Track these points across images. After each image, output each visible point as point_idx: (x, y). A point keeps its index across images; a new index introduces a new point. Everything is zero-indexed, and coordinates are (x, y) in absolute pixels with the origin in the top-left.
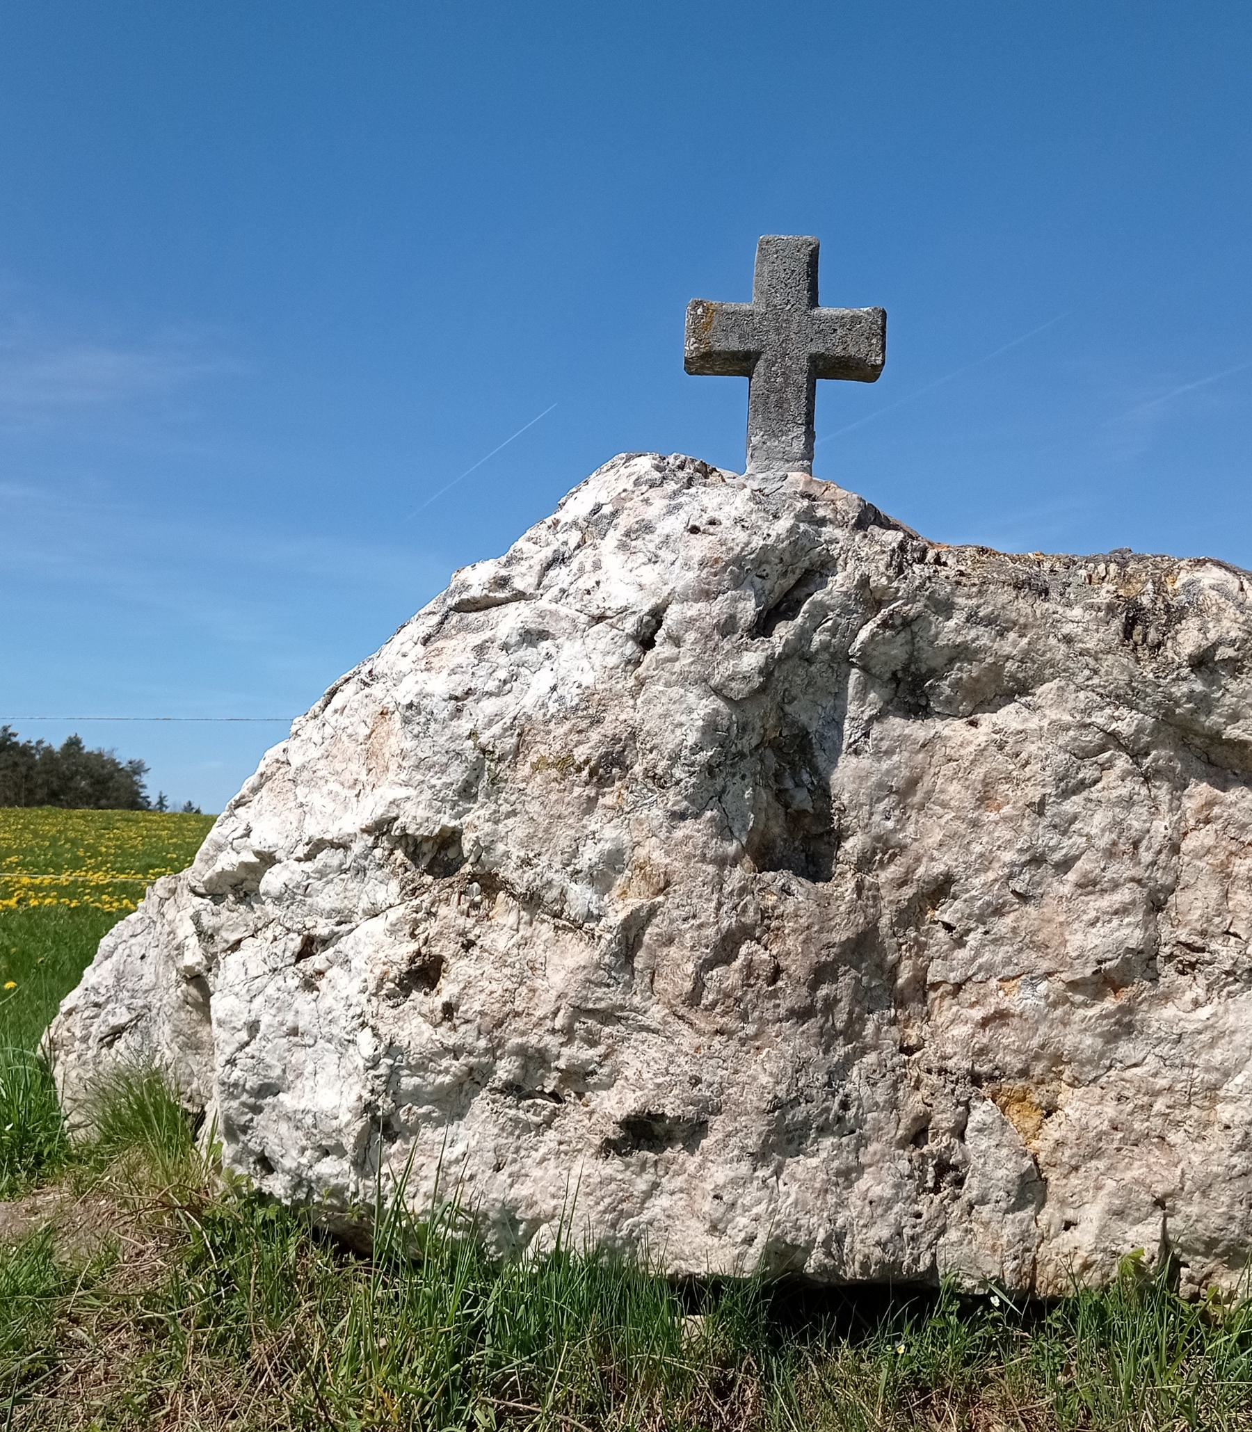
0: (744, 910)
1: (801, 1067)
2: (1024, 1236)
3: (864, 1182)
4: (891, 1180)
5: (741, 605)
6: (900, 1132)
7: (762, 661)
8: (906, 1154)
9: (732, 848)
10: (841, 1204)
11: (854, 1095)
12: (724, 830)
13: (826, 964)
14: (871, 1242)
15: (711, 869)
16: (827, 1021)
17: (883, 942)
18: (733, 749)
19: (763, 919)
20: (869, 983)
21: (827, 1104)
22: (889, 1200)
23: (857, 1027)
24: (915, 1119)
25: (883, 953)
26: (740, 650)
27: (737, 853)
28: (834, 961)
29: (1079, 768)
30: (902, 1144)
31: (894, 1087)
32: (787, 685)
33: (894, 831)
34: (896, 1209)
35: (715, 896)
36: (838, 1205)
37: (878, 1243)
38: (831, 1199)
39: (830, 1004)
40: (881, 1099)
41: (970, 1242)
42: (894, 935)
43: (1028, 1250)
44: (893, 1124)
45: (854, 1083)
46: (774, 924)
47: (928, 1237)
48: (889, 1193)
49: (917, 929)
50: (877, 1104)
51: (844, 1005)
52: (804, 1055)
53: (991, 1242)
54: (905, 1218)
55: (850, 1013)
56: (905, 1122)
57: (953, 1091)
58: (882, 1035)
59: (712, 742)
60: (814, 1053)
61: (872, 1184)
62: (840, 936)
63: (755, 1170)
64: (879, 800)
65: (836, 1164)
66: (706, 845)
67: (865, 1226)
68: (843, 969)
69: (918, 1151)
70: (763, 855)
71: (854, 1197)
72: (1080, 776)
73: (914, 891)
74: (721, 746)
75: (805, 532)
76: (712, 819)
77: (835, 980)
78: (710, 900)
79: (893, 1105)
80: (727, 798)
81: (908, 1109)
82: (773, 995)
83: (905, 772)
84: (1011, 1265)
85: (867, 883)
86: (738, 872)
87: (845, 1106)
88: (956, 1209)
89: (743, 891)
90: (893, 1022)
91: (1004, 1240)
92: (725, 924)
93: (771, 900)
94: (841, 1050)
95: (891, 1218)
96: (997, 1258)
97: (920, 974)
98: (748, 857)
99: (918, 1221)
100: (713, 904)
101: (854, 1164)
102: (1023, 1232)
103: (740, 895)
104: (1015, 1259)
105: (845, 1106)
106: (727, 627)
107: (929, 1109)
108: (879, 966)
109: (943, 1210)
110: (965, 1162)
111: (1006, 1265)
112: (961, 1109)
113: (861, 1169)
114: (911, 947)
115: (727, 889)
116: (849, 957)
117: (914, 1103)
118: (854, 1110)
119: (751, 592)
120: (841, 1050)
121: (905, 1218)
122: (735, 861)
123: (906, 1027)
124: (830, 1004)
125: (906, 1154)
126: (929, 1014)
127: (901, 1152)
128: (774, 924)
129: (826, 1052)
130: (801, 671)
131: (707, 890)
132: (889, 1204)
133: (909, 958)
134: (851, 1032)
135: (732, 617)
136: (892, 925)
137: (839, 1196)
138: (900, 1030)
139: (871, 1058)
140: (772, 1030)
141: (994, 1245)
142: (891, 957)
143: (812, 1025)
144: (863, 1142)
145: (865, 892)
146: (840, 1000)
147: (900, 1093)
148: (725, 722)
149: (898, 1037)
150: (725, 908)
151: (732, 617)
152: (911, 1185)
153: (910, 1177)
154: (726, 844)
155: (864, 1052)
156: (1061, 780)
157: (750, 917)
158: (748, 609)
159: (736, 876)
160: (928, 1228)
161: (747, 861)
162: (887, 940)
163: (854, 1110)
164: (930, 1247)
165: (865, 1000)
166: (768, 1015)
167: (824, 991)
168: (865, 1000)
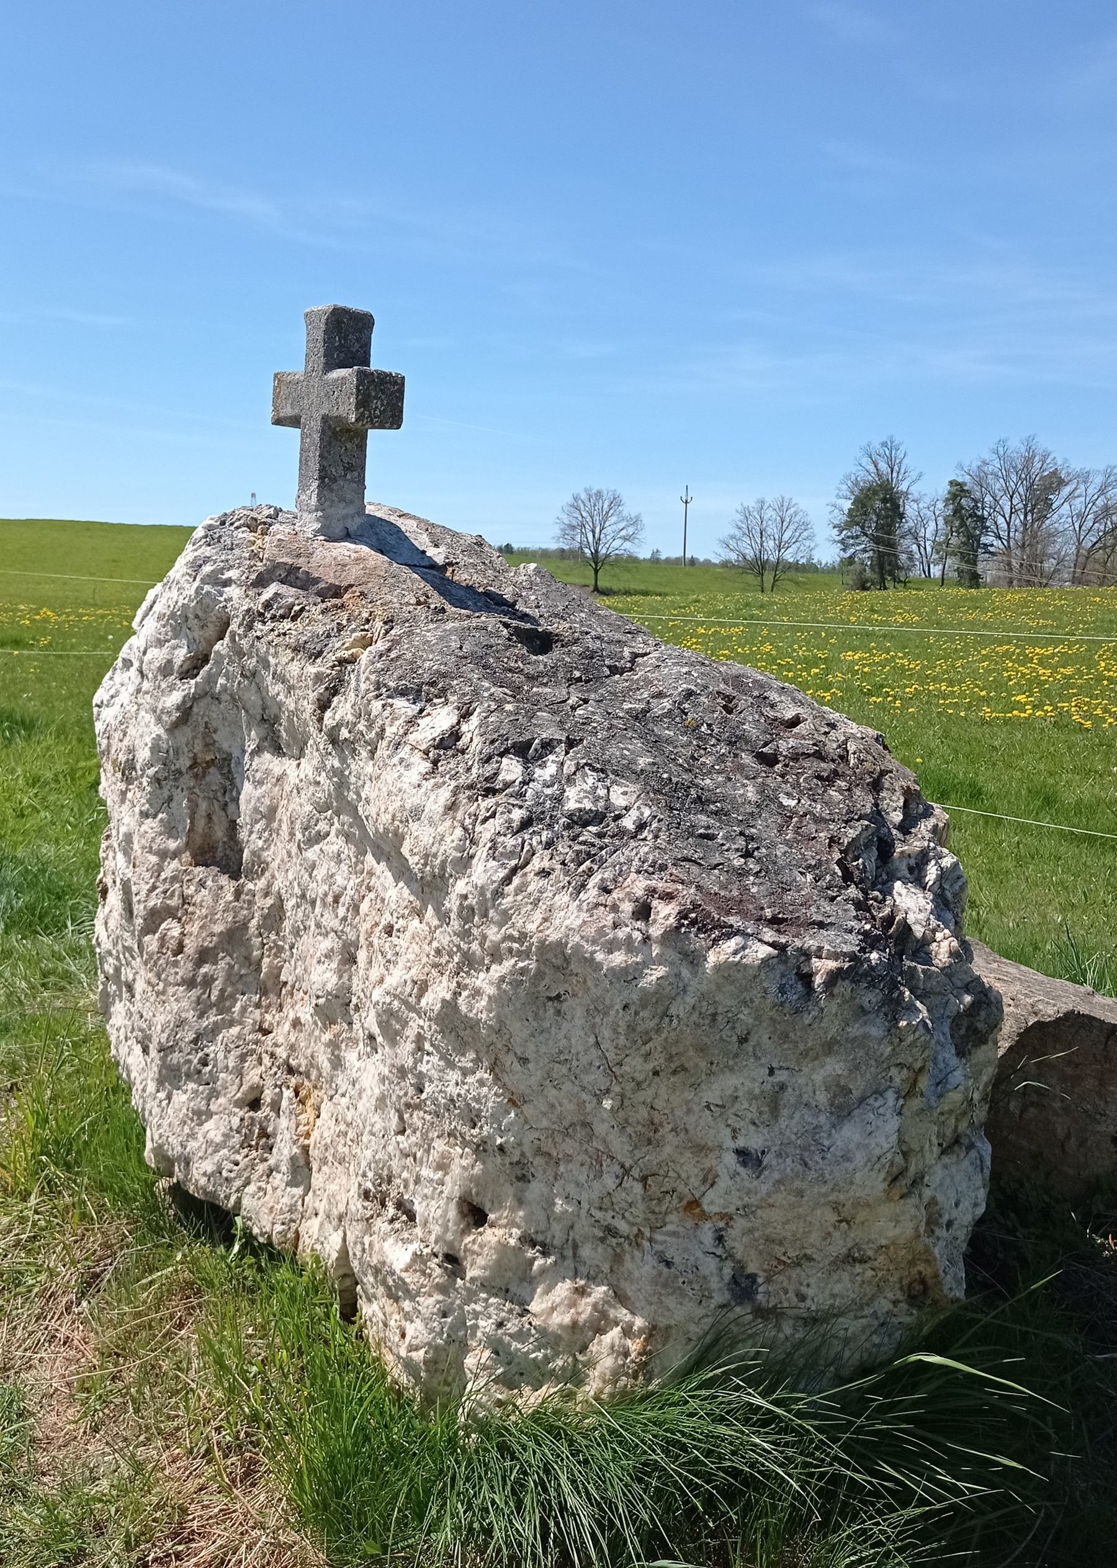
0: (172, 895)
1: (181, 1023)
2: (292, 1209)
3: (209, 1125)
4: (223, 1130)
5: (176, 652)
6: (239, 1095)
7: (180, 699)
8: (241, 1113)
9: (173, 845)
10: (192, 1135)
11: (212, 1056)
12: (170, 830)
13: (207, 948)
14: (201, 1171)
15: (154, 859)
16: (204, 993)
17: (249, 940)
18: (173, 768)
19: (184, 903)
20: (240, 970)
21: (190, 1057)
22: (217, 1144)
23: (228, 1003)
24: (252, 1088)
25: (249, 948)
26: (172, 688)
27: (178, 848)
28: (215, 947)
29: (318, 821)
30: (239, 1104)
31: (243, 1058)
32: (206, 719)
33: (262, 849)
34: (221, 1153)
35: (152, 881)
36: (188, 1135)
37: (205, 1174)
38: (187, 1130)
39: (208, 982)
40: (231, 1065)
41: (259, 1199)
42: (260, 935)
43: (294, 1221)
44: (235, 1087)
45: (215, 1050)
46: (191, 909)
47: (238, 1183)
48: (219, 1139)
49: (277, 934)
50: (227, 1067)
51: (218, 985)
52: (183, 1015)
53: (271, 1204)
54: (225, 1162)
55: (222, 991)
56: (244, 1088)
57: (276, 1073)
58: (247, 1015)
59: (157, 761)
60: (190, 1015)
61: (213, 1129)
62: (218, 928)
63: (158, 1091)
64: (257, 822)
65: (192, 1104)
66: (153, 839)
67: (201, 1158)
68: (221, 955)
69: (251, 1113)
70: (203, 854)
71: (201, 1132)
72: (317, 828)
73: (272, 902)
74: (165, 764)
75: (208, 593)
76: (161, 820)
77: (215, 963)
78: (147, 883)
79: (240, 1073)
80: (173, 805)
81: (248, 1078)
82: (175, 964)
83: (267, 801)
84: (279, 1228)
85: (246, 889)
86: (175, 864)
87: (204, 1062)
88: (261, 1168)
89: (174, 879)
90: (258, 1006)
91: (278, 1207)
92: (151, 904)
93: (191, 890)
94: (213, 1018)
95: (217, 1157)
96: (271, 1218)
97: (275, 971)
98: (188, 854)
99: (235, 1168)
100: (148, 887)
101: (204, 1108)
102: (291, 1205)
103: (172, 883)
104: (283, 1224)
105: (204, 1062)
106: (166, 669)
107: (262, 1082)
108: (247, 958)
109: (252, 1166)
110: (274, 1135)
111: (276, 1226)
112: (277, 1090)
113: (210, 1114)
114: (271, 948)
115: (163, 876)
116: (226, 946)
117: (253, 1076)
118: (210, 1067)
119: (184, 641)
120: (213, 1018)
121: (225, 1162)
122: (175, 855)
123: (266, 1012)
124: (208, 982)
125: (241, 1113)
126: (281, 1006)
127: (237, 1110)
128: (191, 909)
129: (201, 1016)
130: (213, 707)
131: (148, 874)
132: (218, 1148)
133: (269, 956)
134: (223, 1004)
135: (169, 662)
136: (259, 927)
137: (192, 1129)
138: (261, 1014)
139: (235, 1030)
140: (171, 990)
141: (272, 1208)
142: (256, 953)
143: (195, 993)
144: (214, 1094)
145: (243, 896)
146: (216, 979)
147: (247, 1064)
148: (165, 746)
149: (258, 1018)
150: (157, 891)
151: (169, 662)
152: (237, 1139)
153: (238, 1132)
154: (171, 841)
155: (231, 1024)
156: (306, 829)
157: (174, 902)
158: (181, 654)
159: (172, 867)
160: (239, 1176)
161: (186, 857)
162: (254, 939)
163: (210, 1067)
164: (238, 1191)
165: (237, 983)
166: (171, 979)
167: (204, 970)
168: (237, 983)
